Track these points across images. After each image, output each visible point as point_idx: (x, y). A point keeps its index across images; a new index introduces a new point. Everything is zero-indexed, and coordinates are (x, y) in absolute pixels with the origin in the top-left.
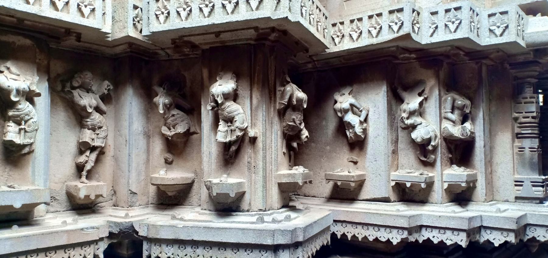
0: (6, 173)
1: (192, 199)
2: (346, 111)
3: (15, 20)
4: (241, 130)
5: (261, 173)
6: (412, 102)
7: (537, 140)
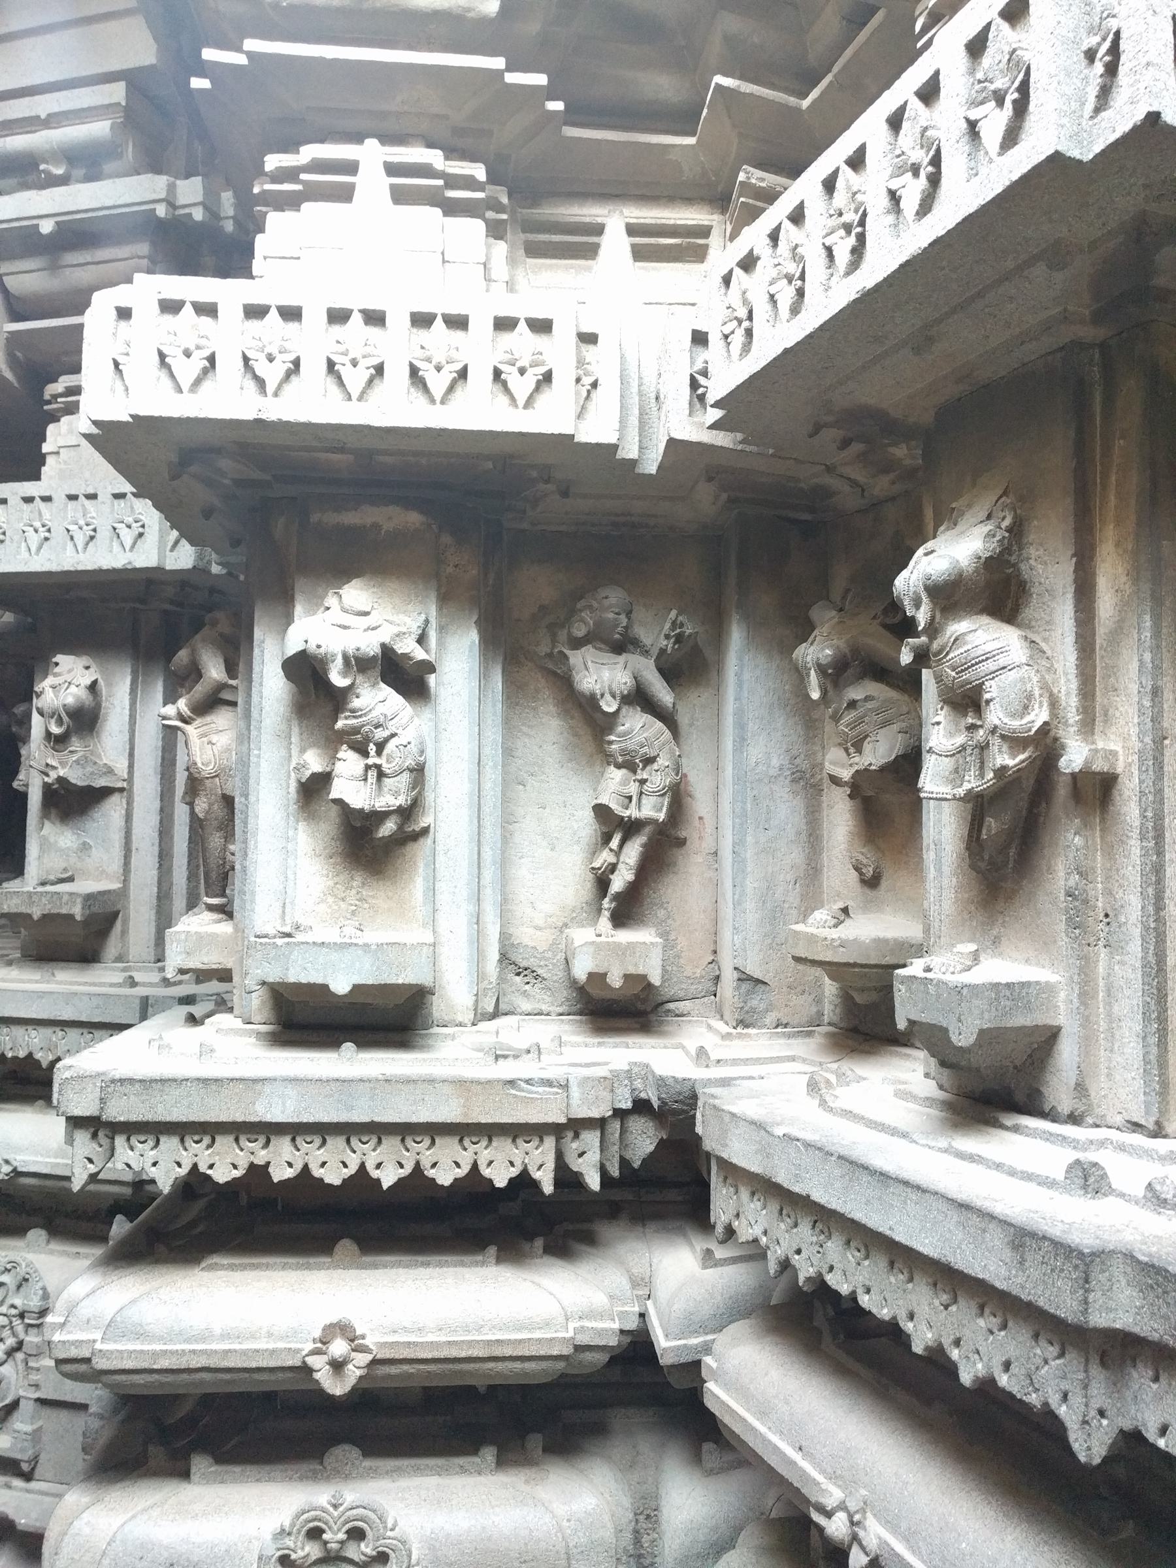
0: (354, 892)
4: (1015, 741)
5: (1135, 947)
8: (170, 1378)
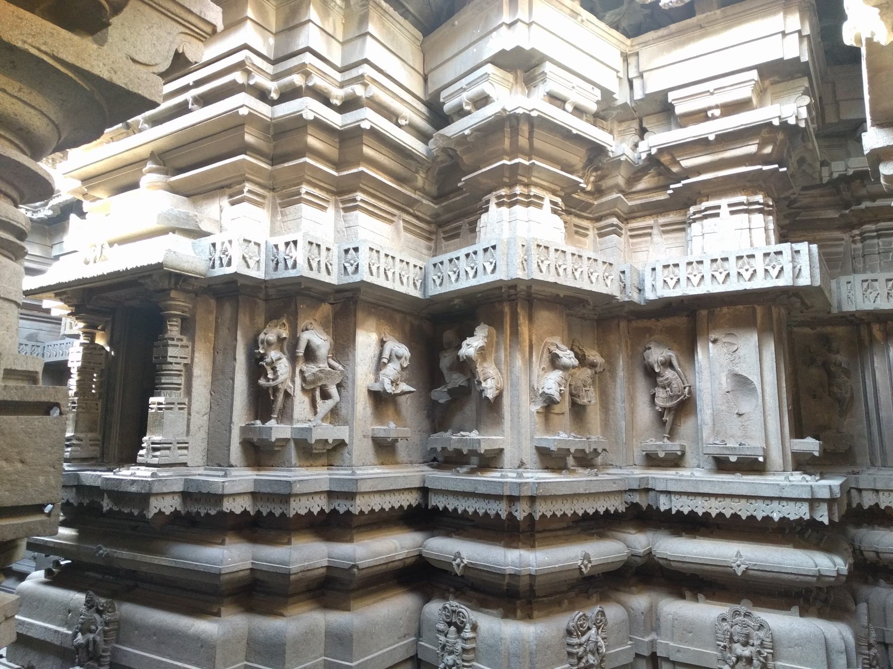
8: (685, 566)
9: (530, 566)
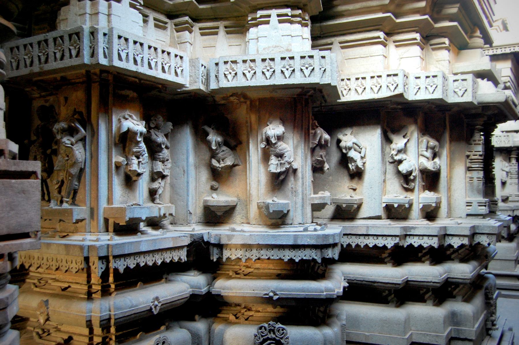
1: (235, 218)
2: (350, 149)
3: (137, 80)
6: (399, 142)
7: (482, 172)
8: (127, 318)
9: (141, 304)
